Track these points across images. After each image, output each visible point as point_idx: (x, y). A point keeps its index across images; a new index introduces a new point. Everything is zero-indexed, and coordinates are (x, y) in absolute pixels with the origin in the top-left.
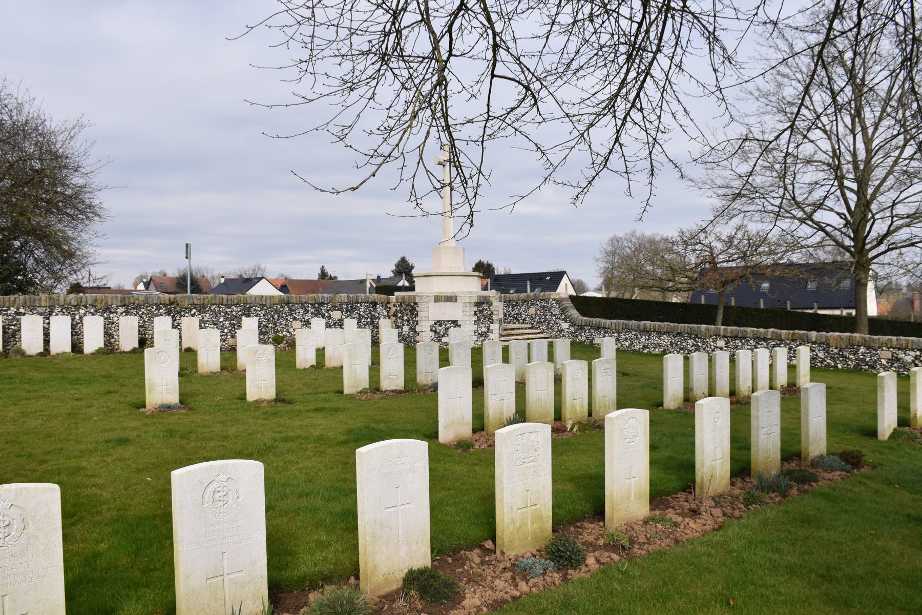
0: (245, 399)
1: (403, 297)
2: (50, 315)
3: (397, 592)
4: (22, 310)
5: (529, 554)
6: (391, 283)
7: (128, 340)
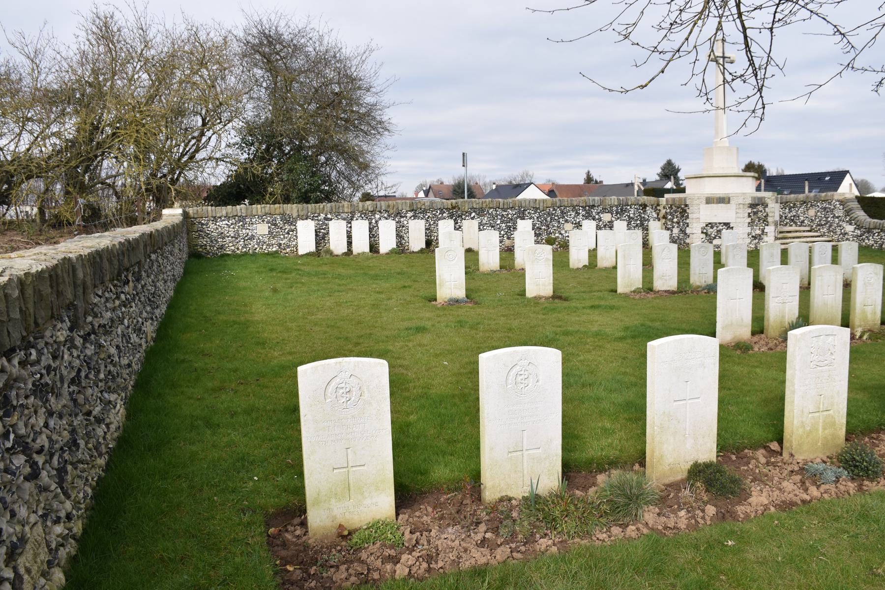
0: (525, 295)
1: (674, 199)
2: (352, 219)
3: (682, 481)
4: (329, 216)
5: (819, 460)
6: (658, 186)
7: (416, 242)
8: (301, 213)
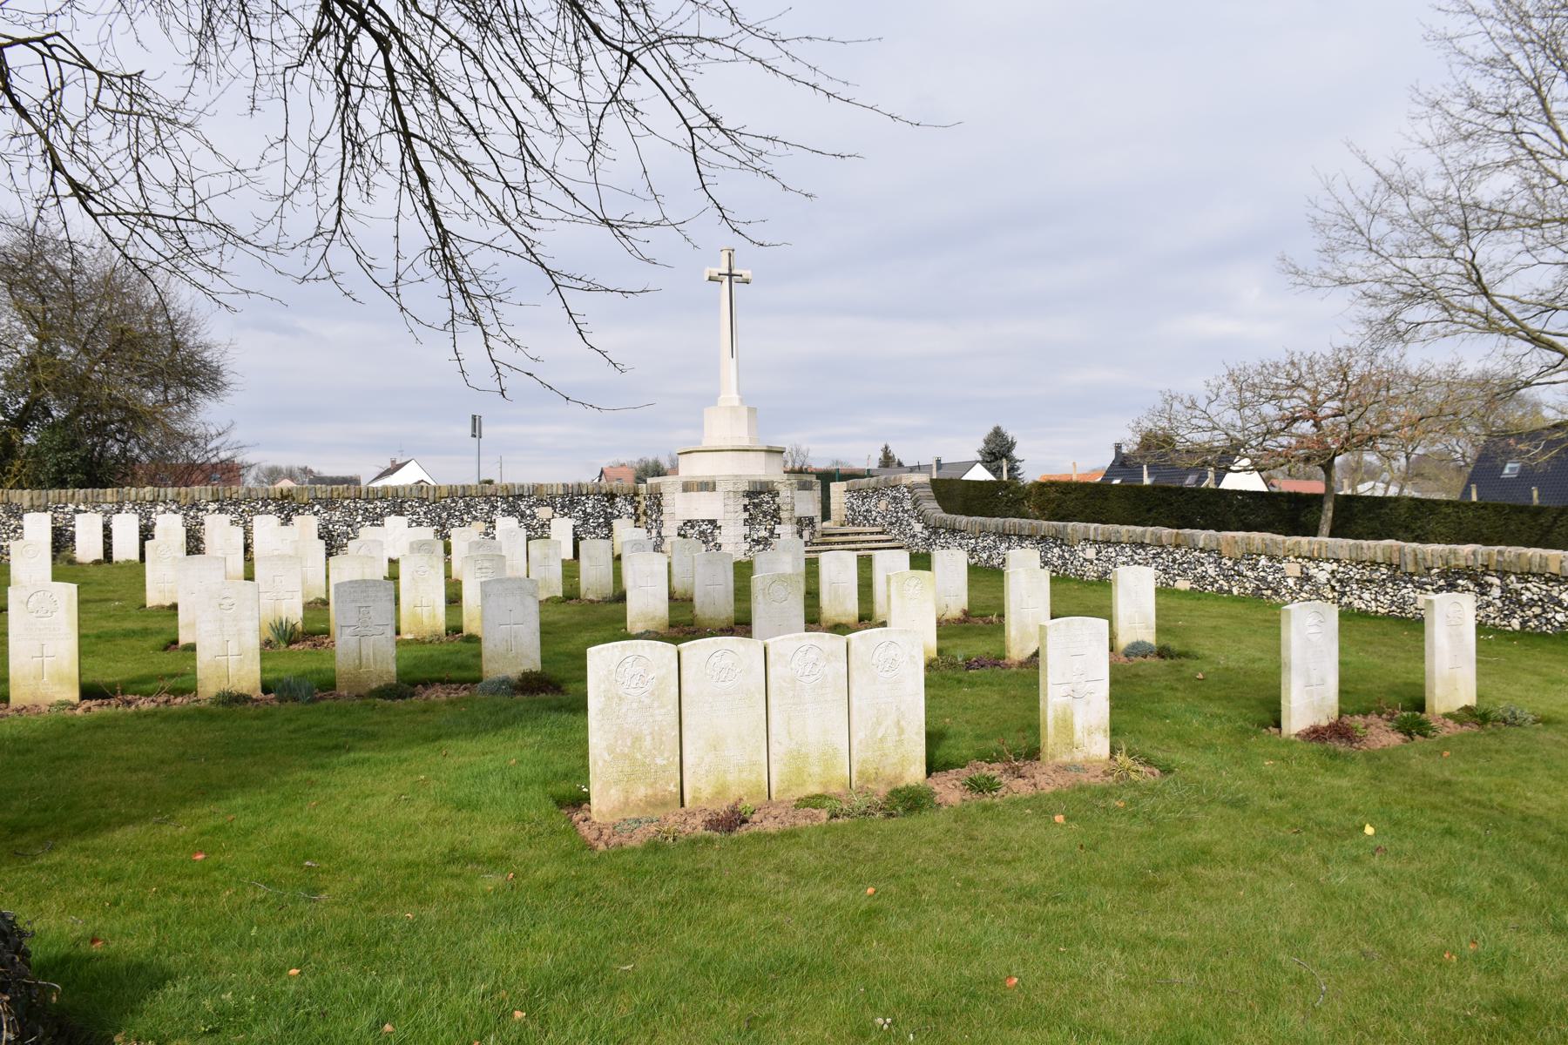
4: (82, 507)
8: (36, 503)
